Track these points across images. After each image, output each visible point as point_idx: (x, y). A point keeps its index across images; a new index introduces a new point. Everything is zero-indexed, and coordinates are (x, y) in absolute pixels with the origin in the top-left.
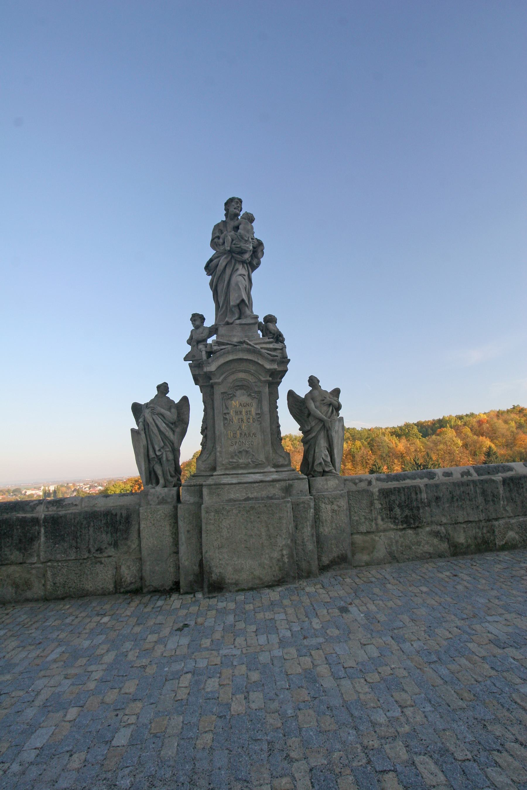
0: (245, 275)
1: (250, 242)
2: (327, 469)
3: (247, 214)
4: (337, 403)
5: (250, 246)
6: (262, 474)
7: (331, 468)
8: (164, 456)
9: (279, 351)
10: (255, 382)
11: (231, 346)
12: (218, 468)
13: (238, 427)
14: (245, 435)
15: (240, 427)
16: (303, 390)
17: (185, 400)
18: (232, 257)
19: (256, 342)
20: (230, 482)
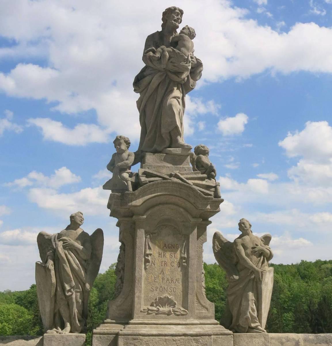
0: (179, 98)
1: (190, 62)
2: (253, 325)
3: (187, 28)
4: (268, 252)
5: (189, 66)
6: (184, 326)
7: (257, 324)
8: (74, 296)
9: (213, 189)
10: (183, 221)
11: (160, 179)
12: (135, 315)
13: (161, 270)
14: (168, 280)
15: (162, 271)
16: (231, 236)
17: (99, 233)
18: (167, 75)
19: (189, 176)
20: (149, 333)
